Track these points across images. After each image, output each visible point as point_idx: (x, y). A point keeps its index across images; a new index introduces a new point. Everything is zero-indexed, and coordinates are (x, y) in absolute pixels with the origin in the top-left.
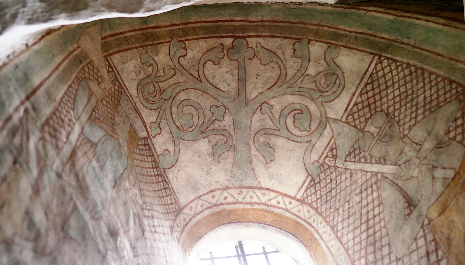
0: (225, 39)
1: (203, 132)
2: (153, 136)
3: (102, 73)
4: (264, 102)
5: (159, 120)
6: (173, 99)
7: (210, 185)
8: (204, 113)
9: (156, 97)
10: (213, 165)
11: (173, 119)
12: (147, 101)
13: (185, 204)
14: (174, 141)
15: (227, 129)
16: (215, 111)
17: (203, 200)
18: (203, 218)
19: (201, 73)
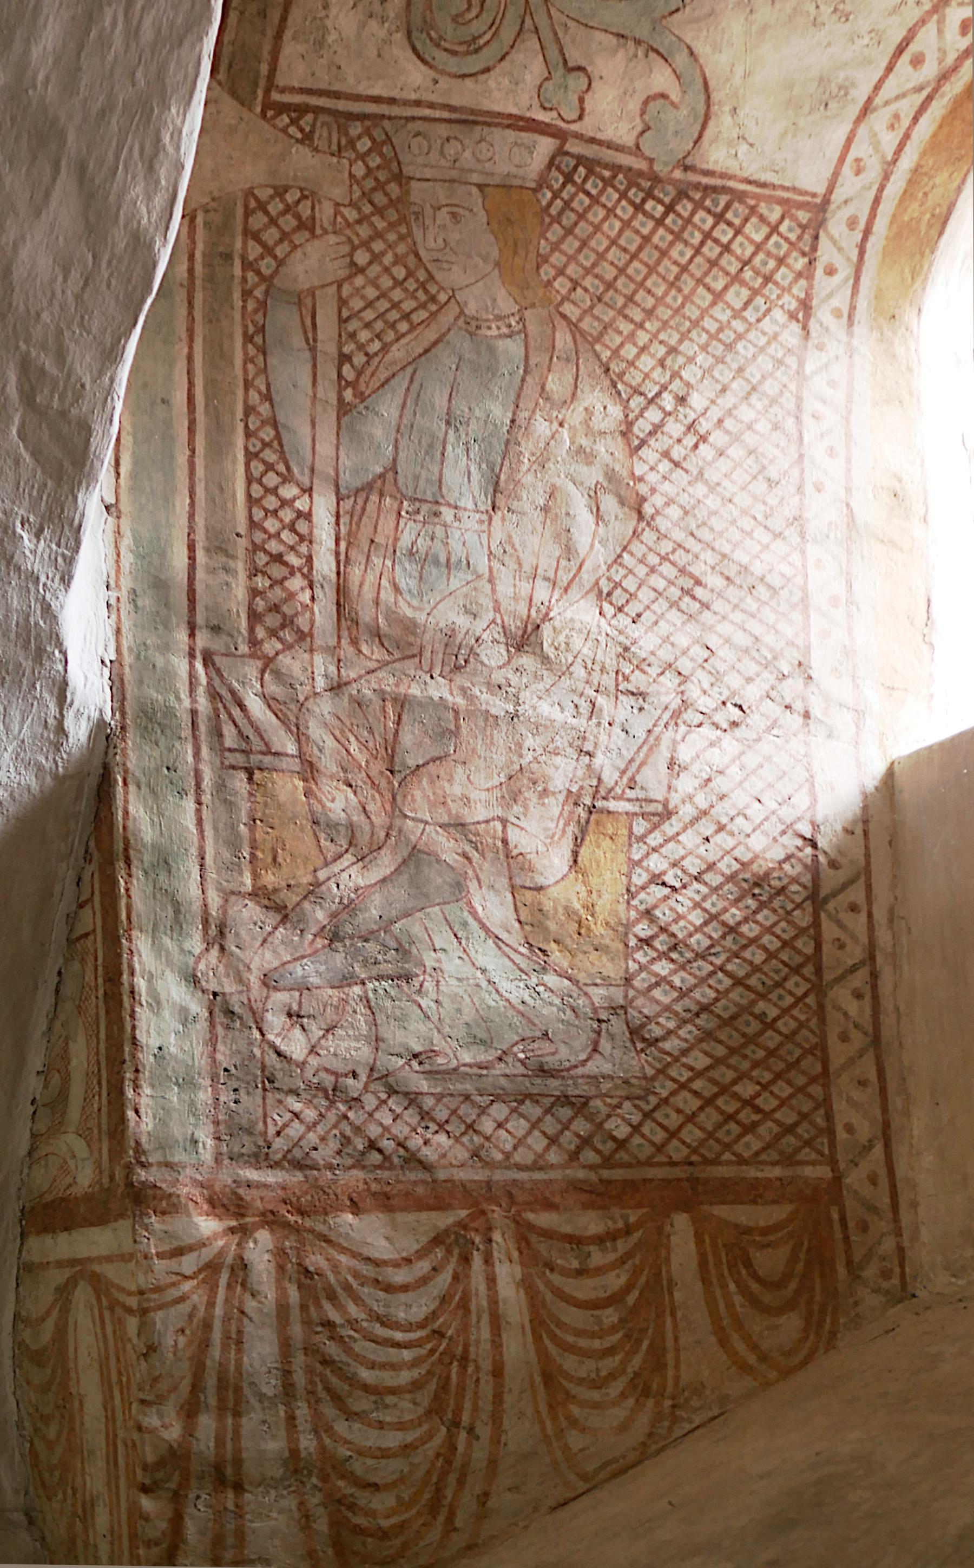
2: (575, 116)
3: (296, 178)
7: (877, 36)
12: (473, 46)
17: (887, 103)
18: (924, 153)
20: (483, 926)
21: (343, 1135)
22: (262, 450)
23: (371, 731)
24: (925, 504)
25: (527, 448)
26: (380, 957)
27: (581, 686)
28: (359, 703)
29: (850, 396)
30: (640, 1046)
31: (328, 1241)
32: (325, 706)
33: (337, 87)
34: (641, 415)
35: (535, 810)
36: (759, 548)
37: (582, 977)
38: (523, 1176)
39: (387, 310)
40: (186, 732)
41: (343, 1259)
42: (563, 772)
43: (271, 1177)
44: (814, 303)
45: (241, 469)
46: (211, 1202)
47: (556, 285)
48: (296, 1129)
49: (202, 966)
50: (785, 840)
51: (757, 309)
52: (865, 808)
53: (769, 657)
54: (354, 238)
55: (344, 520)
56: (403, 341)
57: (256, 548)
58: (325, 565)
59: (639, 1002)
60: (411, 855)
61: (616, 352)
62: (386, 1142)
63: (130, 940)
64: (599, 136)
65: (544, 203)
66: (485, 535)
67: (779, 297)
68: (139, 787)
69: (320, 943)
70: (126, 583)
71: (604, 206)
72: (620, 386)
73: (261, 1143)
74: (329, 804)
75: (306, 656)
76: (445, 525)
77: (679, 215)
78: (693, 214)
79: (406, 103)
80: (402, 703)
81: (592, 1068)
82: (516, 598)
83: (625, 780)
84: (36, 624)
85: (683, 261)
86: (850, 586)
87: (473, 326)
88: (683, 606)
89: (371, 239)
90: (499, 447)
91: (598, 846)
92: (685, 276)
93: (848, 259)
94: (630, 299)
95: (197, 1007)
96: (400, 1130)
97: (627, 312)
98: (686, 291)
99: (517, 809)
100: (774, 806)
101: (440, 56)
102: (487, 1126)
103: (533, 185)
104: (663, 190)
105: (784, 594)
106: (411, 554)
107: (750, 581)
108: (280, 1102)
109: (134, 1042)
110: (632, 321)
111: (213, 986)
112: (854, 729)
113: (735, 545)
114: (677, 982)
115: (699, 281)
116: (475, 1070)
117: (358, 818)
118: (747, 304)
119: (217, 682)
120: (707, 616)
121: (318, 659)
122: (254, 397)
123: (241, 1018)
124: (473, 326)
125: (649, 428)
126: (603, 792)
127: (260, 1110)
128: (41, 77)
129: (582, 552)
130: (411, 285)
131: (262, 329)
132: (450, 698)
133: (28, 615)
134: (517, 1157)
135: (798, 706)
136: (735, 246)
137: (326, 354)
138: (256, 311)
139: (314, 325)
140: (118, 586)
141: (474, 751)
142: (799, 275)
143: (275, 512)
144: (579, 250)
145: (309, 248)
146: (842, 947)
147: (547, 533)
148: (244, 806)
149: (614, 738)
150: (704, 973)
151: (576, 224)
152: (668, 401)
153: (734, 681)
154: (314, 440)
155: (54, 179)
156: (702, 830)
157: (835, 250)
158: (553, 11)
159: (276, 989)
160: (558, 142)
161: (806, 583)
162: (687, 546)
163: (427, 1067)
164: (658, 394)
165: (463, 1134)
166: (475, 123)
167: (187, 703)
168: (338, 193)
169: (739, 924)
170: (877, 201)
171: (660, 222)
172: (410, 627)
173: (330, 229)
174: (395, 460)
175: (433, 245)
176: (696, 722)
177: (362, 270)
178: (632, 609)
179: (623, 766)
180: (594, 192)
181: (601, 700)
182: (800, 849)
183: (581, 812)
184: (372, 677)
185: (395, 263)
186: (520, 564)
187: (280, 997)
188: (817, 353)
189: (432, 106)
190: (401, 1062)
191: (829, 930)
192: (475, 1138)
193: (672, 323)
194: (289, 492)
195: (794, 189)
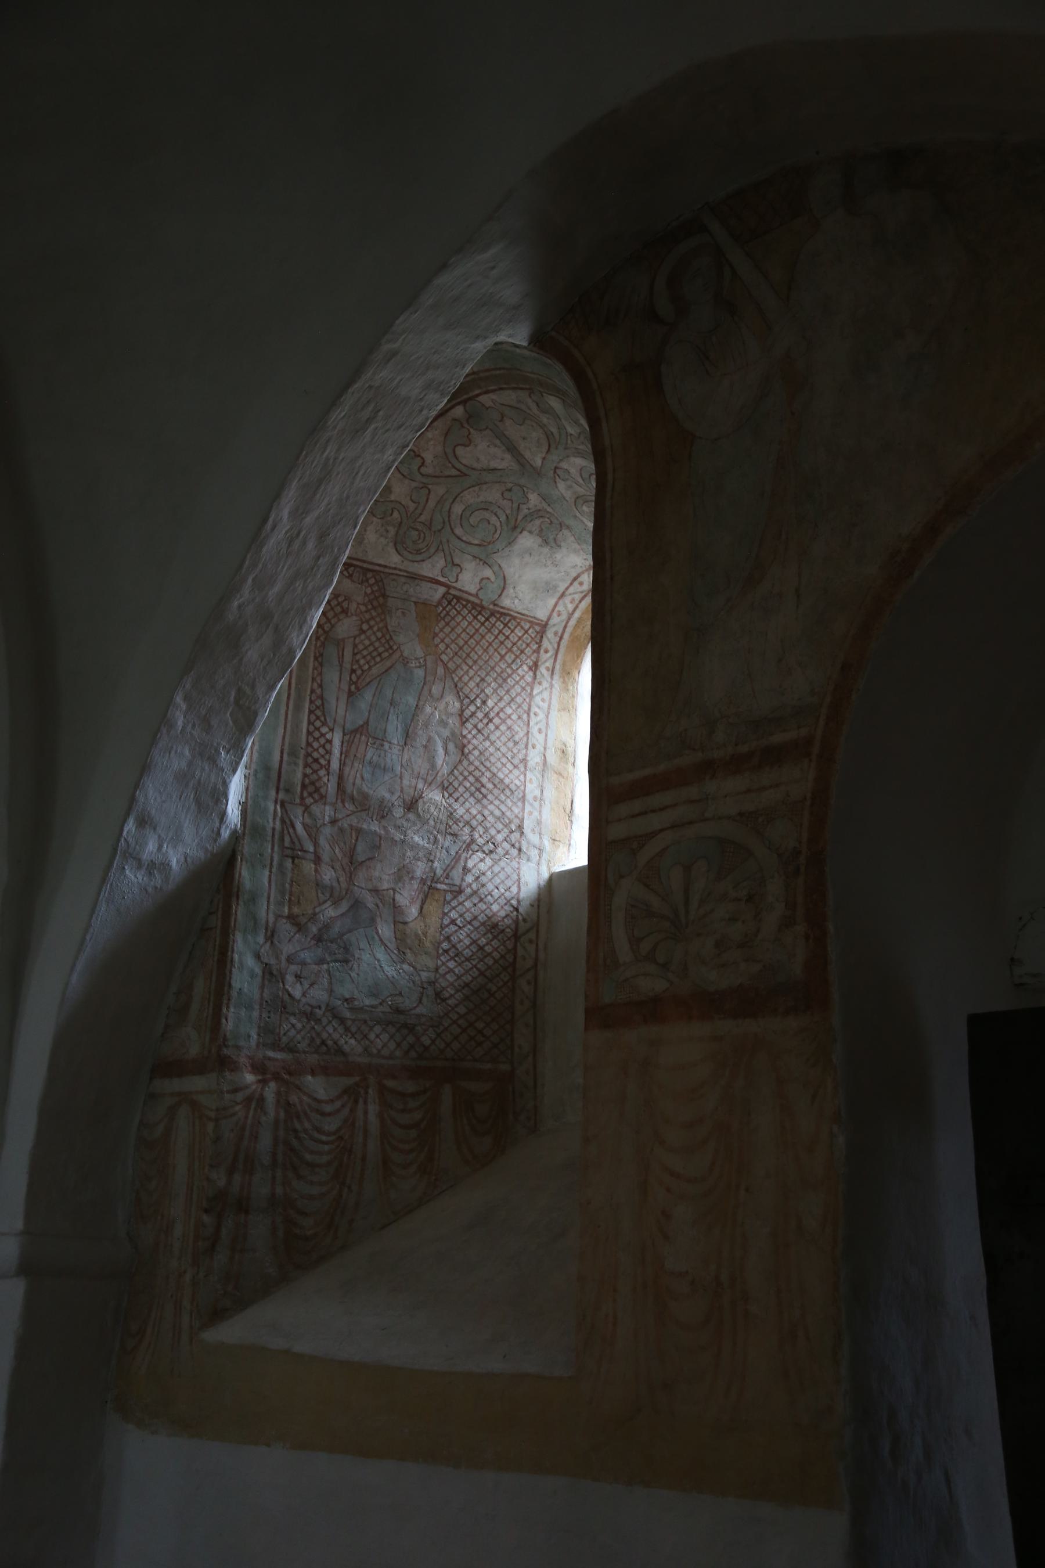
0: (453, 411)
1: (515, 528)
4: (556, 468)
5: (449, 559)
11: (465, 542)
12: (418, 552)
19: (458, 465)
20: (381, 940)
25: (422, 719)
28: (341, 830)
29: (549, 706)
32: (327, 831)
37: (419, 967)
40: (269, 838)
41: (305, 1098)
42: (420, 869)
43: (279, 1056)
45: (306, 718)
48: (292, 1033)
50: (506, 907)
52: (539, 894)
55: (345, 744)
57: (308, 755)
58: (335, 765)
61: (460, 678)
70: (254, 766)
79: (390, 568)
80: (359, 831)
81: (418, 1011)
82: (410, 786)
87: (405, 661)
94: (468, 655)
95: (258, 970)
96: (336, 1036)
99: (400, 885)
100: (503, 891)
101: (406, 553)
102: (372, 1036)
109: (230, 986)
111: (266, 960)
113: (499, 770)
115: (496, 650)
117: (335, 884)
120: (485, 801)
121: (327, 808)
122: (315, 685)
129: (439, 767)
130: (383, 640)
131: (321, 655)
135: (517, 845)
142: (534, 651)
148: (289, 875)
152: (478, 702)
153: (493, 832)
167: (271, 825)
168: (360, 599)
170: (565, 627)
171: (483, 624)
172: (366, 797)
177: (364, 632)
178: (456, 795)
183: (426, 888)
187: (293, 968)
189: (400, 570)
190: (340, 1002)
191: (520, 952)
194: (324, 730)
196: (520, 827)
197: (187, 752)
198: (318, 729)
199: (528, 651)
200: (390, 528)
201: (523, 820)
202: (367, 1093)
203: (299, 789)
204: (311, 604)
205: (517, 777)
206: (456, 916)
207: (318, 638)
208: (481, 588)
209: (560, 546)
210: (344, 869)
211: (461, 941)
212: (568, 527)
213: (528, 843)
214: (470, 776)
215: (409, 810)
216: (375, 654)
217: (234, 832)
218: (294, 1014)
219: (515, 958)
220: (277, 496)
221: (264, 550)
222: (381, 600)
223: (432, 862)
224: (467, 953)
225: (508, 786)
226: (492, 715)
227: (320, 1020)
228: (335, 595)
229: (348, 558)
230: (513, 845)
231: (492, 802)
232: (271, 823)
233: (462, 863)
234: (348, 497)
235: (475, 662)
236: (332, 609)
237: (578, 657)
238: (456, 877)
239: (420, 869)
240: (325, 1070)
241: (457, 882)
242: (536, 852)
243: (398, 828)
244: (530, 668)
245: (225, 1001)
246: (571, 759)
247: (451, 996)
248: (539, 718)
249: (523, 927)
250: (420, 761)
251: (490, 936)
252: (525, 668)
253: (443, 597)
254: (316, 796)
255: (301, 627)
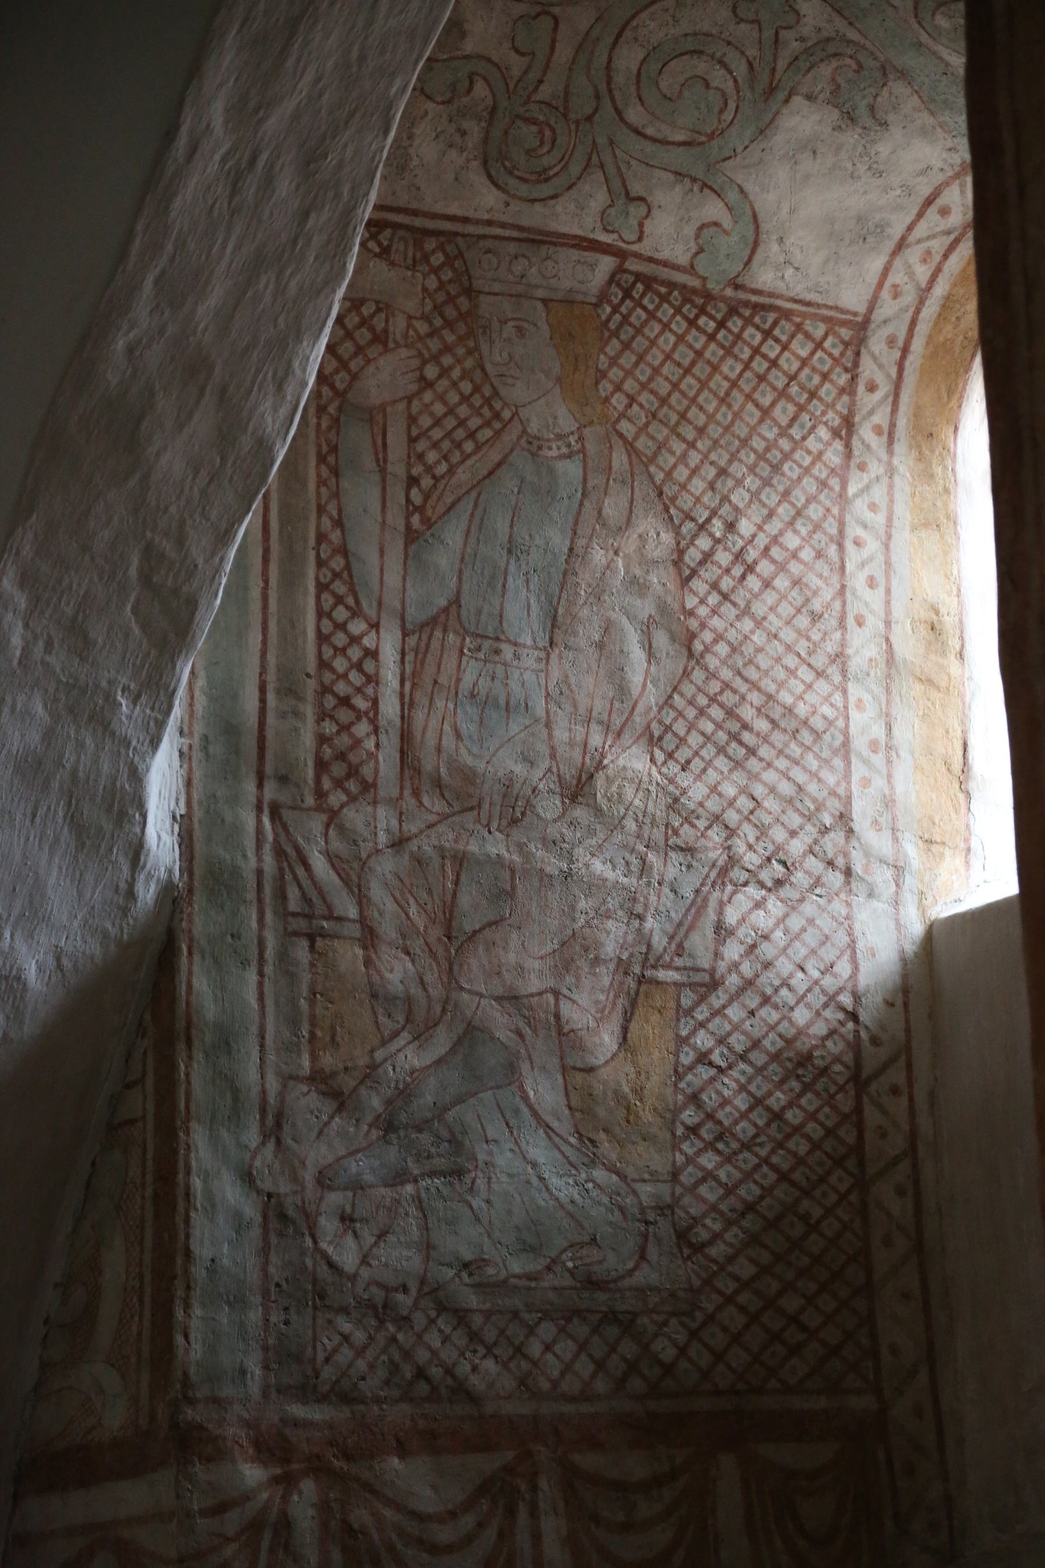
1: (771, 91)
2: (633, 237)
5: (617, 184)
6: (610, 91)
7: (909, 191)
8: (729, 43)
9: (558, 142)
10: (874, 142)
11: (655, 140)
12: (543, 176)
13: (869, 297)
14: (705, 185)
15: (833, 35)
16: (757, 12)
17: (919, 241)
20: (535, 1114)
21: (392, 1362)
22: (332, 581)
23: (430, 892)
24: (962, 638)
25: (585, 578)
26: (433, 1150)
27: (631, 840)
28: (419, 861)
29: (890, 520)
30: (686, 1251)
31: (373, 1491)
32: (386, 866)
33: (414, 205)
34: (692, 543)
35: (587, 982)
36: (802, 687)
37: (631, 1172)
38: (569, 1408)
39: (454, 429)
40: (251, 895)
41: (388, 1513)
42: (613, 937)
43: (317, 1413)
44: (857, 419)
45: (312, 601)
46: (257, 1444)
47: (614, 401)
48: (345, 1355)
49: (258, 1163)
50: (828, 1013)
51: (802, 426)
52: (905, 976)
53: (812, 807)
54: (425, 352)
55: (410, 657)
56: (469, 463)
57: (325, 690)
58: (390, 708)
59: (686, 1200)
60: (465, 1033)
61: (669, 474)
62: (434, 1370)
63: (187, 1133)
64: (657, 256)
65: (604, 317)
66: (543, 675)
67: (824, 413)
68: (203, 958)
69: (375, 1134)
70: (199, 729)
71: (660, 321)
72: (672, 511)
73: (310, 1372)
74: (388, 975)
75: (370, 809)
76: (505, 664)
77: (730, 331)
78: (743, 329)
79: (478, 222)
80: (461, 860)
81: (639, 1278)
82: (571, 744)
83: (673, 946)
84: (123, 787)
85: (733, 376)
86: (889, 729)
87: (534, 445)
88: (730, 751)
89: (441, 353)
90: (558, 578)
91: (647, 1021)
92: (735, 392)
93: (888, 376)
94: (683, 416)
95: (251, 1211)
96: (449, 1355)
97: (680, 430)
98: (736, 408)
99: (569, 979)
100: (816, 974)
101: (512, 182)
102: (535, 1349)
103: (594, 300)
104: (715, 307)
105: (827, 737)
106: (473, 696)
107: (794, 724)
108: (330, 1322)
109: (188, 1253)
110: (684, 440)
111: (267, 1186)
112: (894, 888)
113: (781, 685)
114: (722, 1175)
115: (748, 397)
116: (524, 1282)
117: (415, 991)
118: (793, 420)
119: (283, 839)
120: (753, 764)
121: (382, 812)
122: (326, 523)
123: (294, 1223)
124: (534, 445)
125: (699, 556)
126: (652, 961)
127: (310, 1332)
128: (202, 326)
129: (636, 691)
130: (477, 400)
131: (334, 449)
132: (507, 855)
133: (116, 779)
134: (564, 1387)
135: (840, 861)
136: (782, 362)
137: (395, 476)
138: (330, 428)
139: (384, 444)
140: (191, 733)
141: (528, 914)
142: (842, 391)
143: (343, 650)
144: (636, 364)
145: (381, 362)
146: (884, 1135)
147: (602, 672)
148: (306, 978)
149: (663, 899)
150: (749, 1167)
151: (633, 338)
152: (717, 527)
153: (779, 834)
154: (382, 570)
155: (198, 402)
156: (748, 1002)
157: (875, 367)
158: (617, 151)
159: (330, 1188)
160: (618, 260)
161: (847, 726)
162: (734, 685)
163: (477, 1278)
164: (708, 520)
165: (511, 1358)
166: (543, 242)
167: (253, 862)
168: (411, 306)
169: (783, 1109)
170: (913, 323)
171: (712, 337)
172: (470, 777)
173: (402, 342)
174: (459, 592)
175: (498, 359)
176: (742, 879)
177: (430, 385)
178: (683, 754)
179: (671, 930)
180: (651, 307)
181: (651, 857)
182: (842, 1024)
183: (631, 983)
184: (432, 832)
185: (462, 378)
186: (575, 707)
187: (335, 1199)
188: (859, 473)
189: (503, 225)
190: (451, 1273)
191: (871, 1116)
192: (523, 1363)
193: (722, 442)
194: (357, 627)
195: (836, 308)
196: (844, 818)
197: (39, 709)
198: (342, 627)
199: (827, 391)
200: (468, 124)
201: (848, 801)
202: (534, 1488)
203: (310, 773)
204: (297, 332)
205: (827, 699)
206: (710, 1043)
207: (321, 410)
208: (701, 250)
209: (885, 124)
210: (433, 955)
211: (725, 1102)
212: (903, 74)
213: (867, 854)
214: (712, 706)
215: (574, 798)
216: (460, 434)
217: (167, 889)
218: (345, 1310)
219: (860, 1137)
220: (194, 71)
221: (177, 204)
222: (464, 303)
223: (641, 918)
224: (744, 1129)
225: (805, 723)
226: (752, 554)
227: (406, 1319)
228: (353, 303)
229: (377, 207)
230: (830, 863)
231: (769, 765)
232: (253, 859)
233: (712, 915)
234: (362, 58)
235: (701, 431)
236: (349, 335)
237: (950, 393)
238: (700, 951)
239: (613, 937)
240: (431, 1441)
241: (705, 963)
242: (889, 874)
243: (551, 844)
244: (836, 433)
245: (180, 1293)
246: (955, 644)
247: (716, 1236)
248: (866, 552)
249: (873, 1059)
250: (589, 681)
251: (795, 1084)
252: (823, 432)
253: (612, 280)
254: (352, 786)
255: (280, 388)
